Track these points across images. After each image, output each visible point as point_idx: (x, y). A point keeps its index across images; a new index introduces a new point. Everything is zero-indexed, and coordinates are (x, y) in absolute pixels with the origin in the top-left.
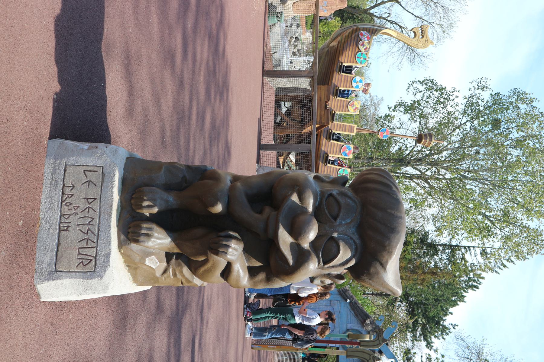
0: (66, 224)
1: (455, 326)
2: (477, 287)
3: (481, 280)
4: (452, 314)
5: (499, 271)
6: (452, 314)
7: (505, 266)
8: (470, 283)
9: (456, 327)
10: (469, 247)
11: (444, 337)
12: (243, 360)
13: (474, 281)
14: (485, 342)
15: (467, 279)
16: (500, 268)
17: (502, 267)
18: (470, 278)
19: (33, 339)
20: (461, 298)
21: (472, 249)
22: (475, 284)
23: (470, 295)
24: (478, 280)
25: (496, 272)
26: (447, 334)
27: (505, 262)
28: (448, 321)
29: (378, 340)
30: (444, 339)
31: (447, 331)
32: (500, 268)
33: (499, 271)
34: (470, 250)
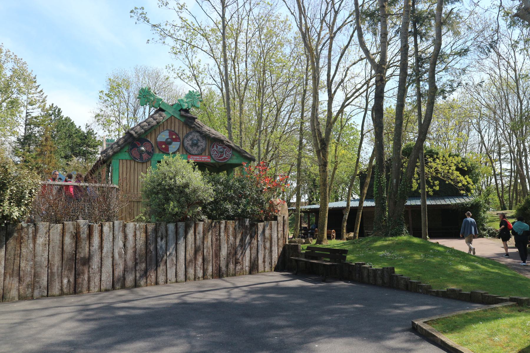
0: (273, 248)
1: (87, 126)
2: (59, 110)
3: (54, 106)
4: (80, 127)
5: (44, 96)
6: (80, 127)
7: (41, 91)
8: (57, 113)
9: (88, 125)
10: (27, 113)
11: (95, 133)
12: (184, 260)
13: (55, 111)
14: (92, 111)
15: (53, 116)
16: (43, 94)
17: (42, 93)
18: (52, 114)
19: (347, 7)
20: (67, 119)
21: (28, 111)
22: (57, 110)
23: (65, 114)
24: (54, 108)
25: (46, 97)
26: (93, 131)
27: (39, 90)
28: (84, 129)
29: (124, 161)
30: (96, 134)
31: (91, 131)
32: (43, 94)
33: (44, 96)
34: (29, 113)
